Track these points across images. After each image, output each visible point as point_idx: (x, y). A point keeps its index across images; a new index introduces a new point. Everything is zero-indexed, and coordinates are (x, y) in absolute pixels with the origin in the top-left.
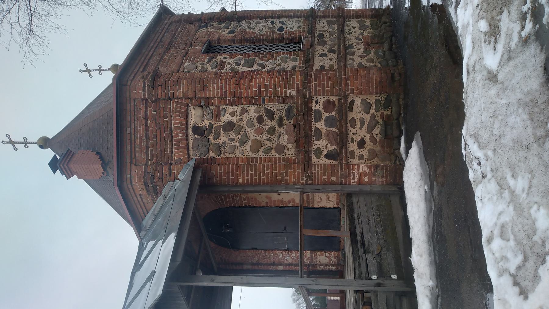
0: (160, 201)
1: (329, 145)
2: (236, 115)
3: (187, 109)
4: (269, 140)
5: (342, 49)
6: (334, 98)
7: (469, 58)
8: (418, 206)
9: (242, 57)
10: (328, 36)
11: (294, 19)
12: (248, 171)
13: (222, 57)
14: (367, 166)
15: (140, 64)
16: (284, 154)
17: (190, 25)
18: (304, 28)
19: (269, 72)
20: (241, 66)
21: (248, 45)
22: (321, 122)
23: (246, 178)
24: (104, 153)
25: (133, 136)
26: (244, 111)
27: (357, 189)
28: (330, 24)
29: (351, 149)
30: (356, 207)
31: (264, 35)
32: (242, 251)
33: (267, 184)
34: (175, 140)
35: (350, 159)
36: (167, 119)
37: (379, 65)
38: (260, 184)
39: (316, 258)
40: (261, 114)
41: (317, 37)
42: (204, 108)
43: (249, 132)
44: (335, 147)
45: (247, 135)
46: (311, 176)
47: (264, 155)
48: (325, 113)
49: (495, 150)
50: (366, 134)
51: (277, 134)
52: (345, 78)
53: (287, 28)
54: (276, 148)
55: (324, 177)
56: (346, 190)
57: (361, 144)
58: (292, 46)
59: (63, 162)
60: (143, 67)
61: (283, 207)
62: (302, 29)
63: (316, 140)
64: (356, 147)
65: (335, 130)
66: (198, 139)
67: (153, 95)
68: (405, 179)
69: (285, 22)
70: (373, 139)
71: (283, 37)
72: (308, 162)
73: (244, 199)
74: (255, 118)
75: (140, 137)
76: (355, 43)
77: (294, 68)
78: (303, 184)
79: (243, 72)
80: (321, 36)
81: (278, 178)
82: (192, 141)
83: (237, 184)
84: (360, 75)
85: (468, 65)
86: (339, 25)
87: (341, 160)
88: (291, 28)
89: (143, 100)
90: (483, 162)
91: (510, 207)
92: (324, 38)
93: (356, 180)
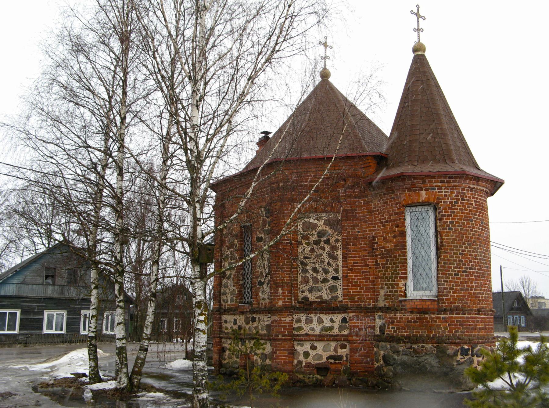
10: (254, 326)
80: (254, 320)
92: (253, 322)
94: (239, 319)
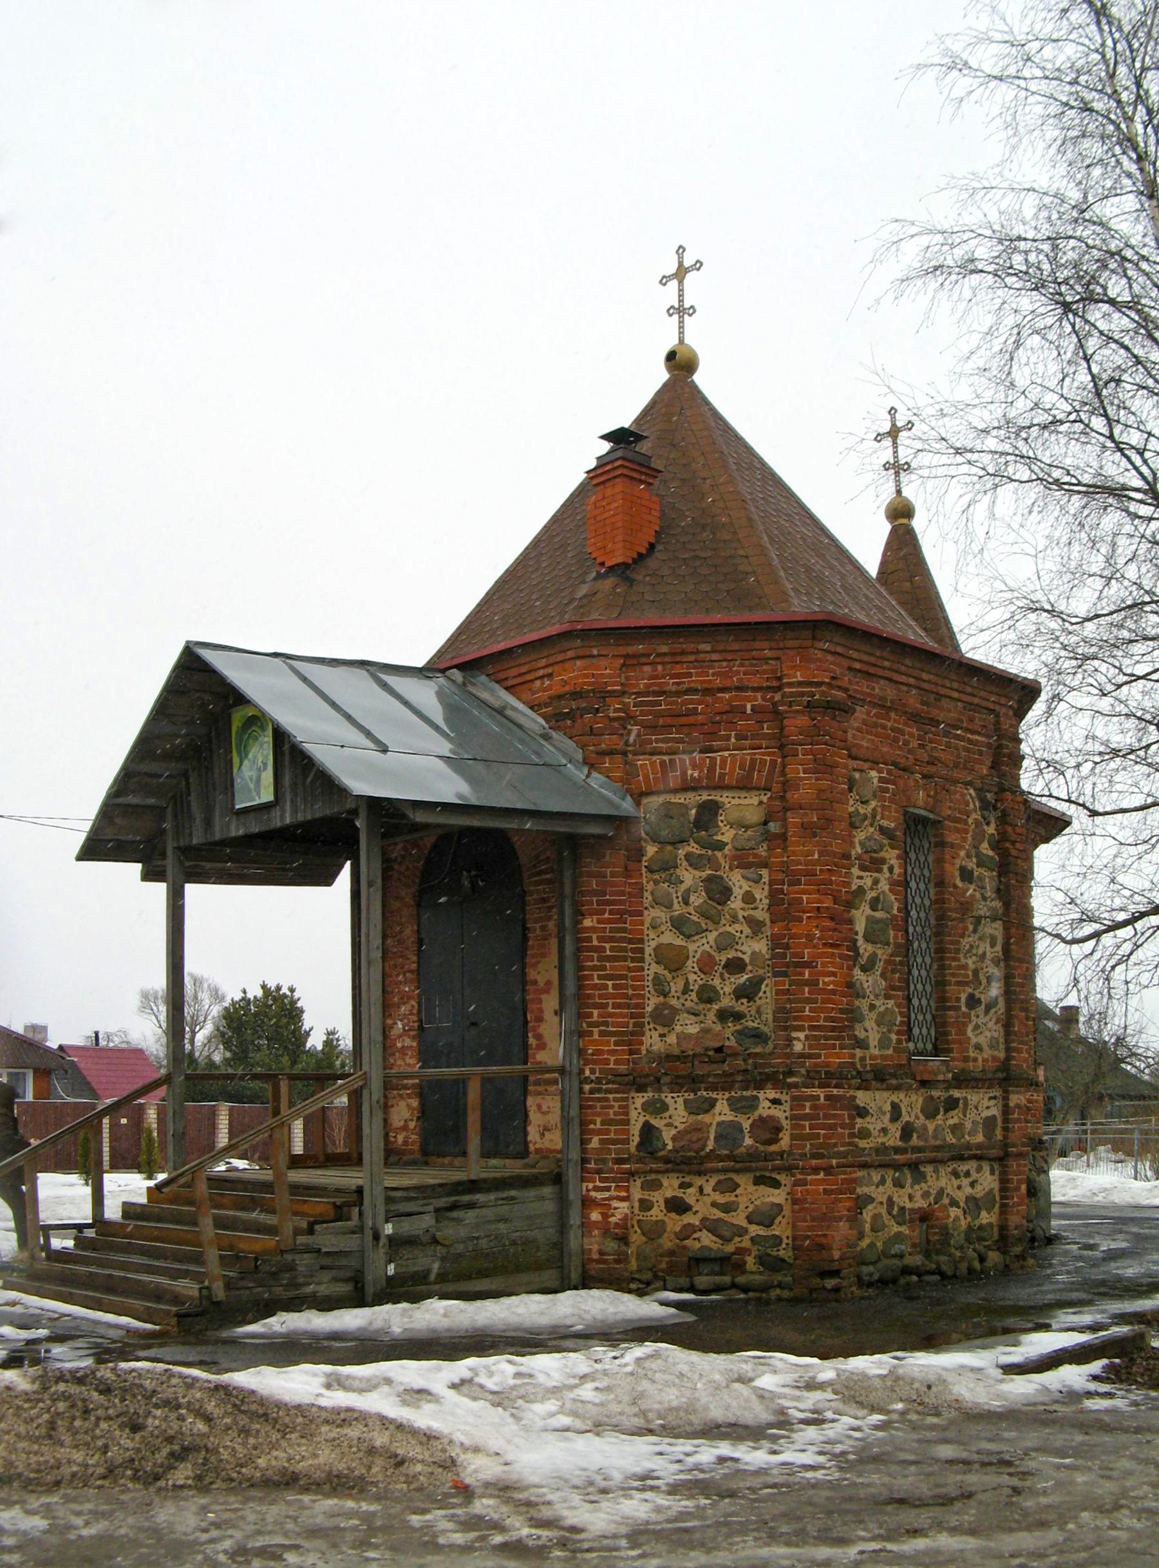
0: (535, 722)
1: (673, 1132)
2: (746, 906)
3: (758, 789)
4: (686, 990)
5: (909, 1156)
6: (785, 1141)
7: (781, 1359)
8: (542, 1314)
9: (895, 912)
10: (951, 1122)
11: (1002, 1034)
12: (611, 940)
13: (893, 862)
14: (625, 1218)
15: (872, 660)
16: (652, 1026)
17: (988, 763)
18: (975, 1060)
19: (850, 985)
20: (869, 912)
21: (933, 921)
22: (729, 1113)
23: (594, 936)
24: (652, 563)
25: (692, 658)
26: (756, 926)
27: (572, 1197)
28: (984, 1124)
29: (665, 1182)
30: (532, 1193)
31: (958, 960)
32: (415, 912)
33: (580, 987)
34: (682, 761)
35: (642, 1179)
36: (733, 740)
37: (864, 1243)
38: (580, 968)
39: (401, 1097)
40: (749, 968)
41: (947, 1095)
42: (761, 829)
43: (704, 941)
44: (670, 1147)
45: (697, 934)
46: (599, 1091)
47: (650, 978)
48: (750, 1121)
49: (632, 1374)
50: (700, 1216)
51: (701, 1006)
52: (832, 1167)
53: (978, 1016)
54: (665, 1005)
55: (599, 1120)
56: (570, 1170)
57: (677, 1206)
58: (929, 1033)
59: (626, 464)
60: (865, 668)
61: (526, 1022)
62: (971, 1054)
63: (686, 1101)
64: (669, 1194)
65: (711, 1145)
66: (685, 814)
67: (790, 706)
68: (595, 1292)
69: (993, 1010)
70: (688, 1232)
71: (950, 1008)
72: (634, 1083)
73: (543, 928)
74: (740, 955)
75: (690, 675)
76: (929, 1187)
77: (862, 1044)
78: (581, 1071)
79: (850, 921)
80: (951, 1104)
81: (596, 1012)
82: (682, 801)
83: (579, 914)
84: (840, 1201)
85: (770, 1357)
86: (979, 1146)
87: (640, 1160)
88: (977, 1027)
89: (780, 679)
90: (617, 1362)
92: (946, 1111)
93: (593, 1194)
94: (906, 1101)
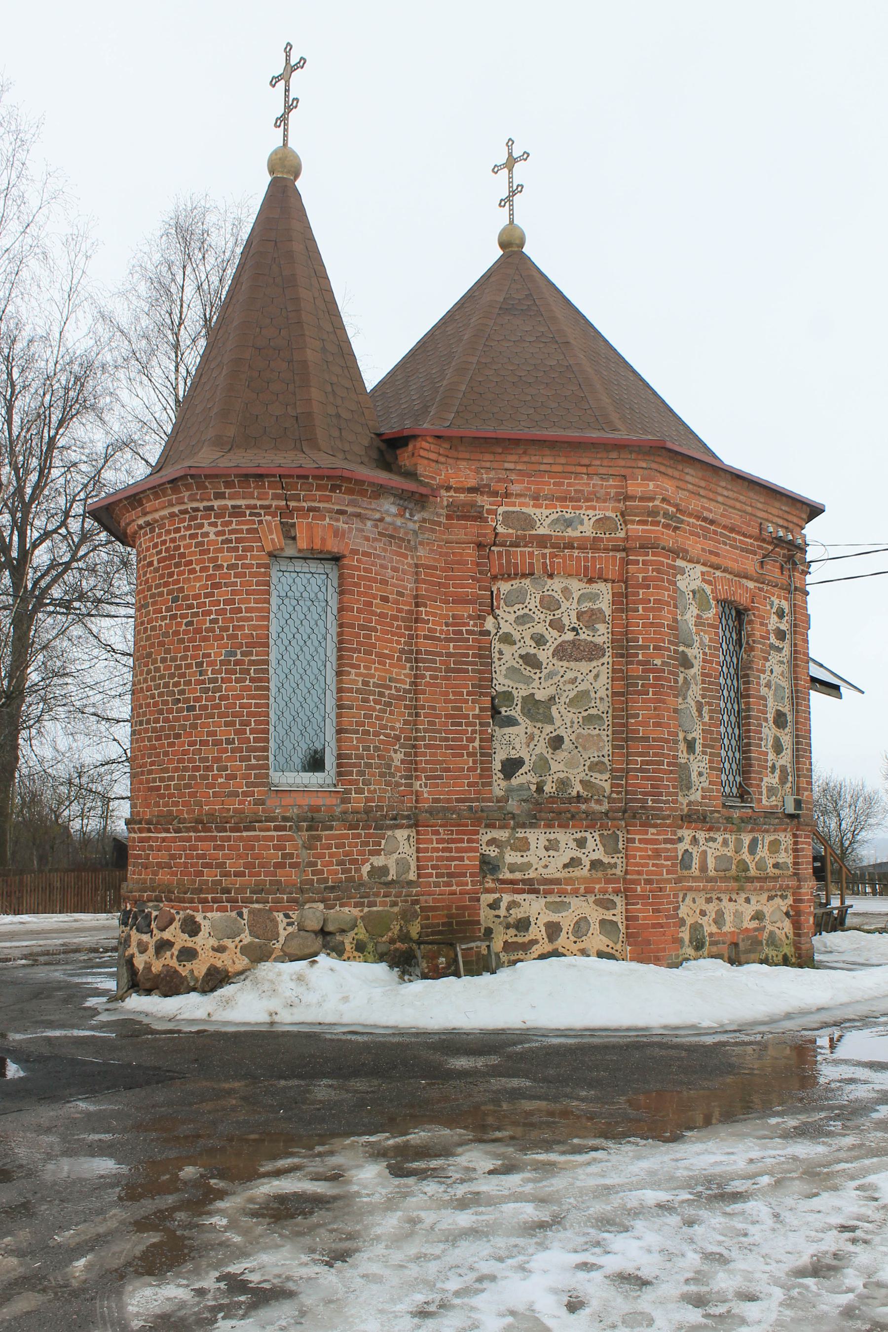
91: (107, 419)
